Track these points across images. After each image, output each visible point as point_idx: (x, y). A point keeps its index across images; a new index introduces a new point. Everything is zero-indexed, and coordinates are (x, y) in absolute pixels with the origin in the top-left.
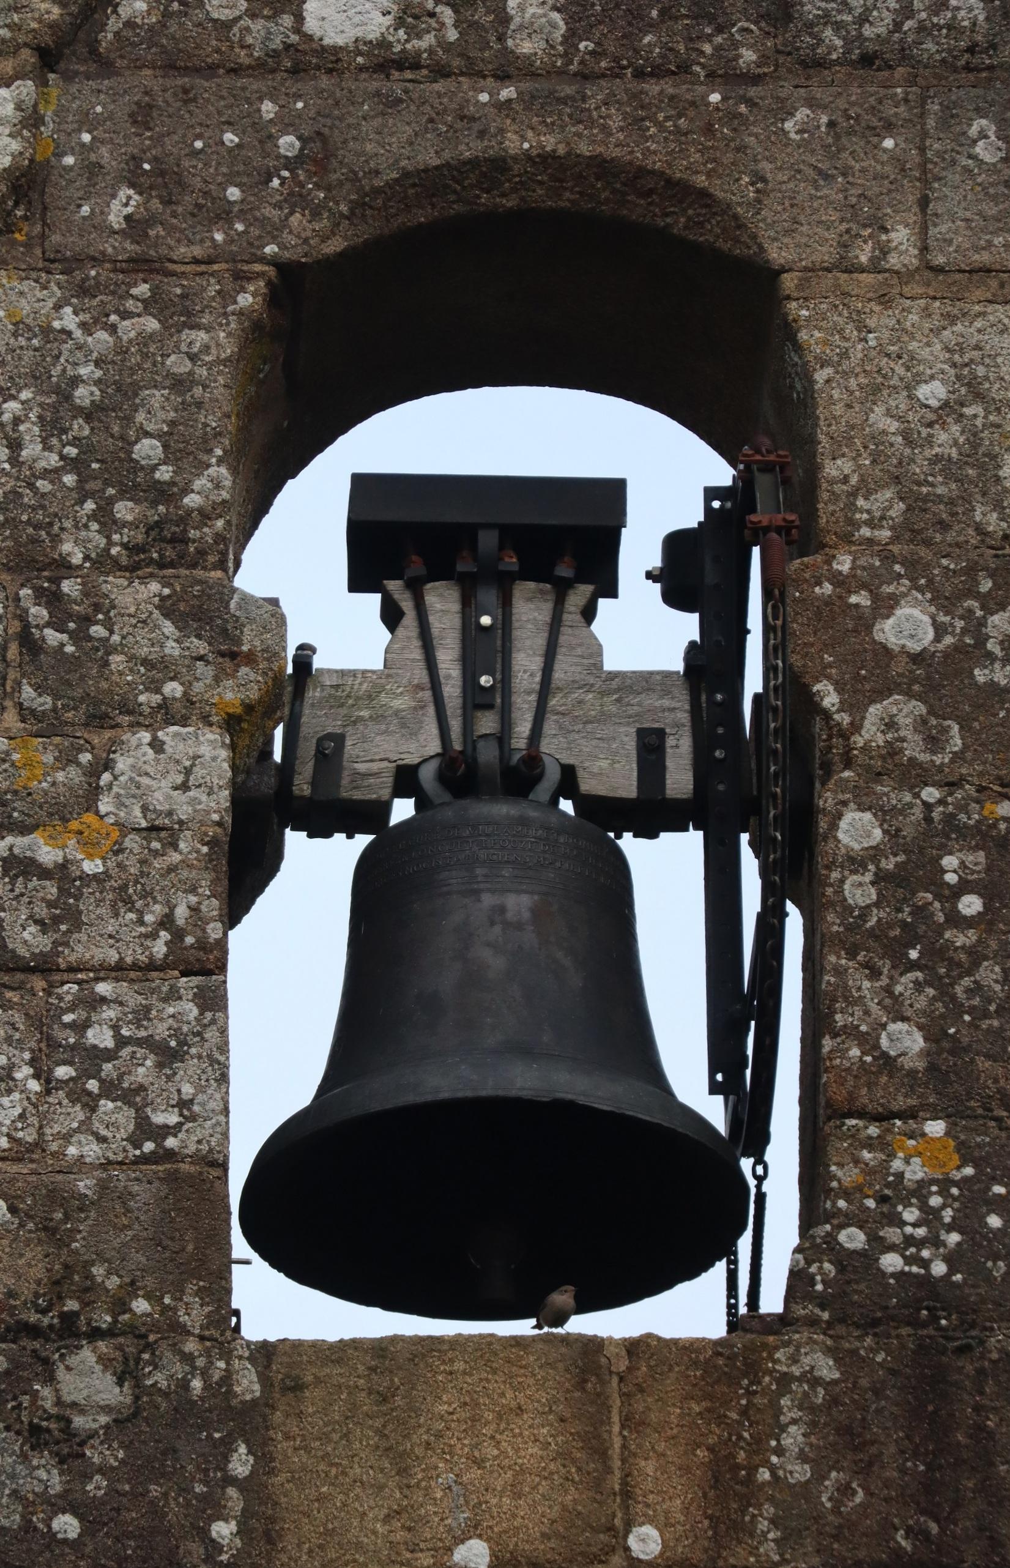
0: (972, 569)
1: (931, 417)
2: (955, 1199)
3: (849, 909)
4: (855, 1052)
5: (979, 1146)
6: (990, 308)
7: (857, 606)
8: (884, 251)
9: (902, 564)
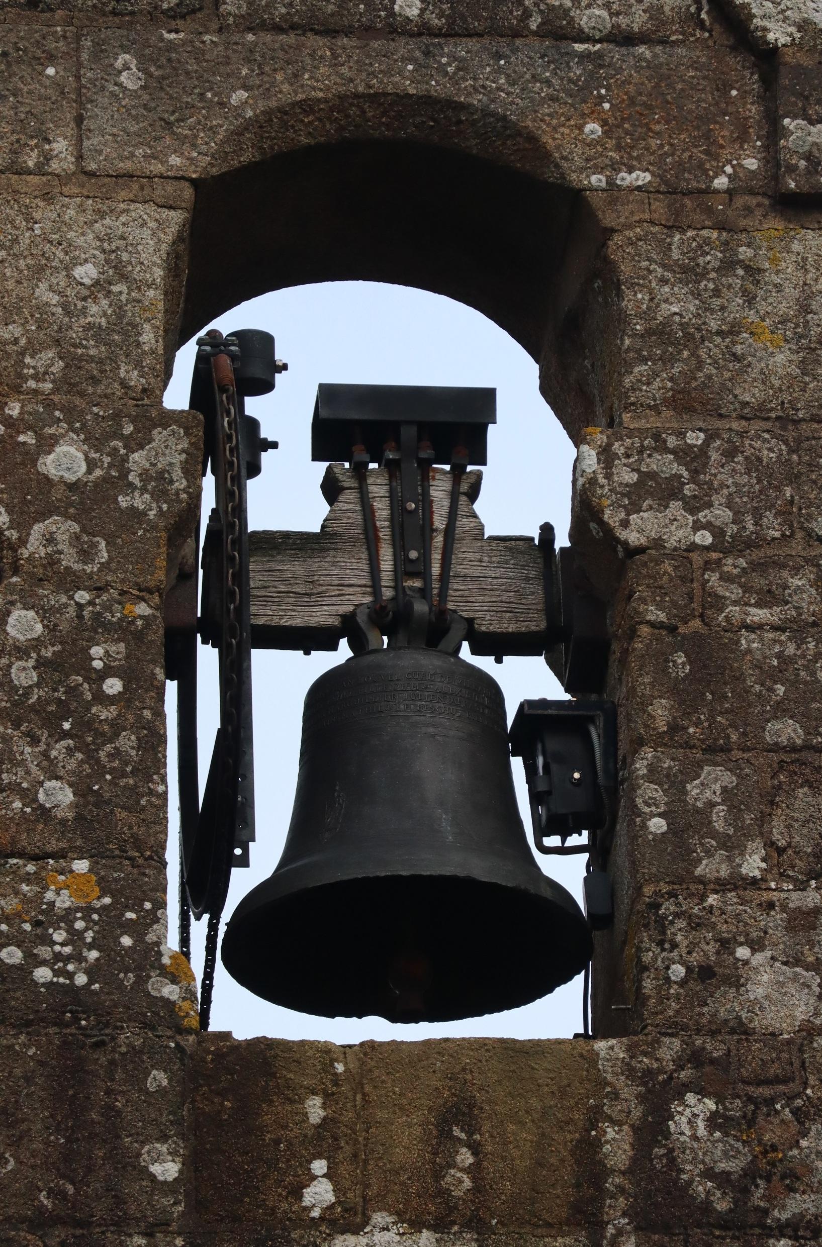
0: (117, 415)
1: (86, 292)
2: (95, 923)
3: (15, 689)
4: (18, 804)
5: (115, 880)
6: (132, 207)
7: (24, 444)
8: (48, 158)
9: (61, 411)
